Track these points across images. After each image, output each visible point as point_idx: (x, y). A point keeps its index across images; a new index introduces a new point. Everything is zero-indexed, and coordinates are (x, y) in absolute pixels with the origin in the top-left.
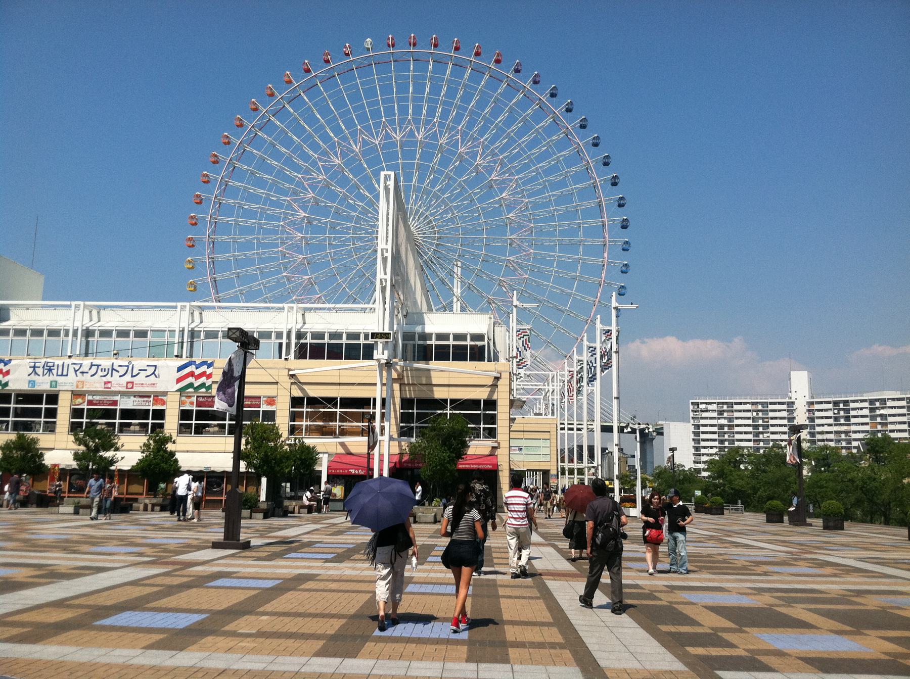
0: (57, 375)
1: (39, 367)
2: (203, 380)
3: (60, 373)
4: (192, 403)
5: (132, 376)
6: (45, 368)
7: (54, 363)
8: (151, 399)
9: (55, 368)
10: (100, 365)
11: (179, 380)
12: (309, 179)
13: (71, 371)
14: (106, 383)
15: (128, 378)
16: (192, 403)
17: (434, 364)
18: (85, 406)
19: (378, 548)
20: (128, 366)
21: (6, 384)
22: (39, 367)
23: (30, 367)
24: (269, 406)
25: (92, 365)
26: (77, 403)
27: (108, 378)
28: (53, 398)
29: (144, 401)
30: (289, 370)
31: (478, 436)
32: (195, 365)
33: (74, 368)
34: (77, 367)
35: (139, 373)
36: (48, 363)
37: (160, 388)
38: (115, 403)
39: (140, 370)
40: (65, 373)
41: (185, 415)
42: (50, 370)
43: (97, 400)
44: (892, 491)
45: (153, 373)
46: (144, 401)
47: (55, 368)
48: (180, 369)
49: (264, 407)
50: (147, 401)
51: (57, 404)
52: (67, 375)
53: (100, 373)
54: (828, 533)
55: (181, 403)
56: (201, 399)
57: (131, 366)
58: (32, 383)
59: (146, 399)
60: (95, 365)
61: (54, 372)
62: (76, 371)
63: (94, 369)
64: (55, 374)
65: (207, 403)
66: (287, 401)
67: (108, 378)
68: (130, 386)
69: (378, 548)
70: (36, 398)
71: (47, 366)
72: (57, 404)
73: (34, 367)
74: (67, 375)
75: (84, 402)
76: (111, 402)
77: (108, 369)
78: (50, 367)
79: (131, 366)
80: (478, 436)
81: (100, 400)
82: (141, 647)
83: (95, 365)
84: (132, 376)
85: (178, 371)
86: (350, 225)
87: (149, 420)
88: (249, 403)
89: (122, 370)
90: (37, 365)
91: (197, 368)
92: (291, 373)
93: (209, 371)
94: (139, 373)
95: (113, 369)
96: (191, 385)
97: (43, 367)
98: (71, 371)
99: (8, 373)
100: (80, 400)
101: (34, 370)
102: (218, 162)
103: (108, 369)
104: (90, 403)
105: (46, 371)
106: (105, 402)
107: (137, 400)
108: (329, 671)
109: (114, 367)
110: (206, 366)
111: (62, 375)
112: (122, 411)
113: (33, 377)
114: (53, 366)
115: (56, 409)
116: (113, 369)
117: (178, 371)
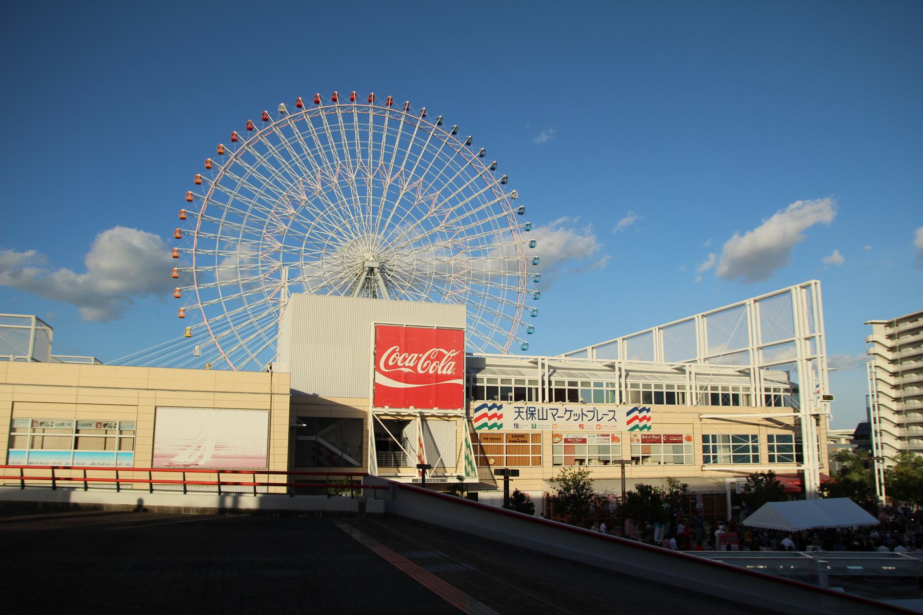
0: (539, 419)
1: (523, 412)
2: (645, 422)
3: (541, 417)
4: (638, 440)
5: (598, 420)
6: (528, 412)
7: (535, 408)
8: (610, 437)
9: (537, 412)
10: (572, 411)
11: (629, 423)
12: (343, 169)
13: (550, 416)
17: (653, 407)
20: (594, 412)
22: (523, 412)
23: (515, 412)
24: (688, 442)
26: (556, 441)
29: (605, 439)
32: (487, 407)
33: (552, 413)
34: (554, 413)
35: (603, 417)
36: (530, 408)
39: (603, 415)
40: (545, 417)
42: (532, 415)
43: (571, 439)
45: (613, 418)
46: (605, 439)
47: (537, 412)
48: (629, 413)
50: (607, 439)
51: (709, 435)
52: (547, 419)
53: (573, 418)
56: (643, 437)
57: (596, 411)
59: (606, 437)
60: (569, 411)
61: (536, 416)
62: (554, 416)
63: (568, 413)
64: (537, 418)
65: (648, 440)
68: (598, 427)
71: (529, 411)
72: (709, 435)
74: (547, 419)
75: (562, 440)
76: (581, 440)
77: (579, 414)
78: (532, 411)
79: (596, 411)
81: (573, 439)
83: (569, 411)
84: (598, 420)
85: (627, 415)
86: (342, 208)
87: (777, 442)
88: (675, 439)
90: (521, 410)
91: (489, 410)
92: (701, 416)
93: (499, 413)
94: (603, 417)
95: (583, 414)
97: (527, 412)
98: (550, 416)
101: (519, 414)
102: (236, 141)
103: (579, 414)
105: (529, 416)
106: (577, 440)
107: (600, 438)
109: (584, 412)
110: (496, 409)
111: (543, 419)
114: (535, 411)
116: (583, 414)
117: (627, 415)
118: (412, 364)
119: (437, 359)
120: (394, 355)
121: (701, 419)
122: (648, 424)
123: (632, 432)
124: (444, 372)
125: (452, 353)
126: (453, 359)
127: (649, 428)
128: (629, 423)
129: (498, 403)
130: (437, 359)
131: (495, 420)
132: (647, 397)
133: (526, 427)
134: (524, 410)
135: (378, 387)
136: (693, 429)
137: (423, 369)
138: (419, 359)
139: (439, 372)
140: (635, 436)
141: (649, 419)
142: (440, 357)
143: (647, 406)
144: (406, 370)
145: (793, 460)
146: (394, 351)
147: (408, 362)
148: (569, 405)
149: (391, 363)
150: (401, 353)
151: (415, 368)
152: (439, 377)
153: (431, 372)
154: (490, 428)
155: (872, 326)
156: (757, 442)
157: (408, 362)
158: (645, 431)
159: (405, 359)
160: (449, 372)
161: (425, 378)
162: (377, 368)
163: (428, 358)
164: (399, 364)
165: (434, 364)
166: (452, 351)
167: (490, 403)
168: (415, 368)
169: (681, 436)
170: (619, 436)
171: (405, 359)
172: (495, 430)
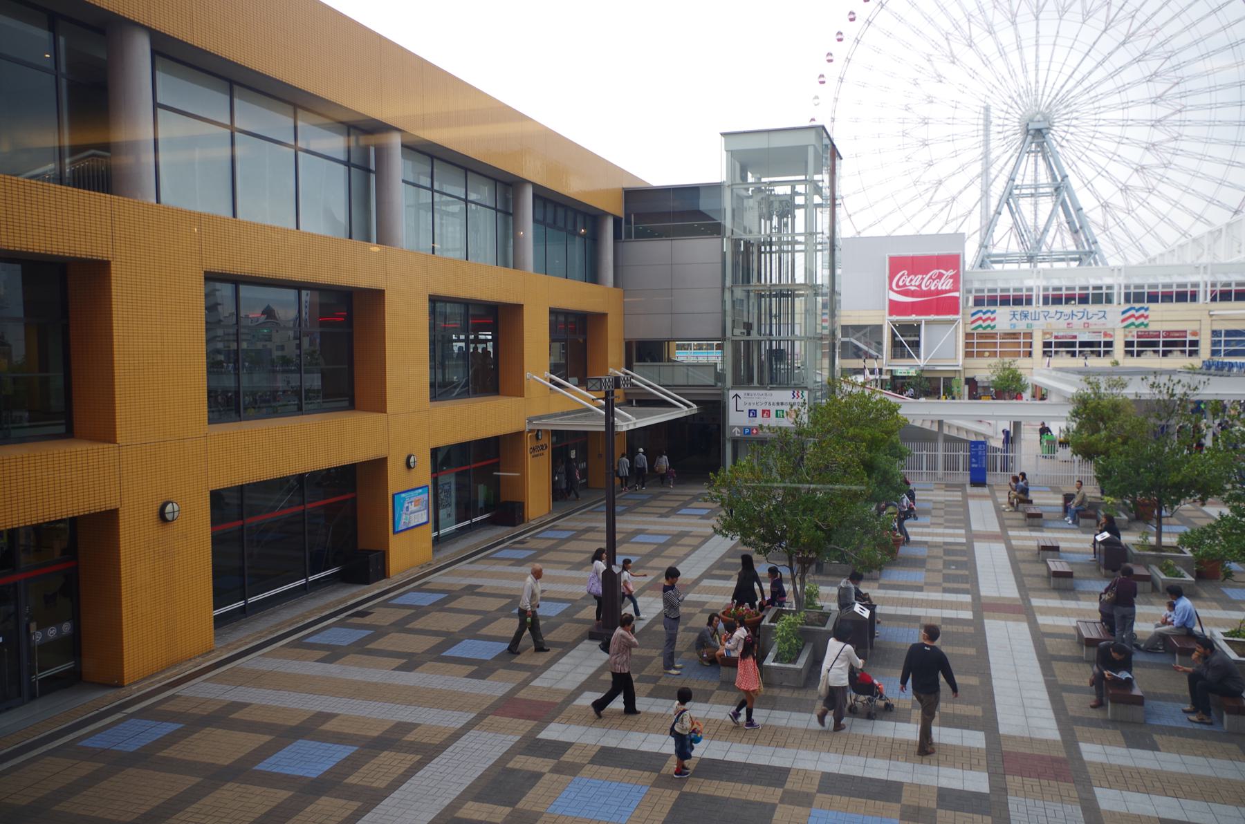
11: (1123, 321)
14: (1068, 324)
15: (1085, 319)
16: (1133, 336)
18: (1053, 340)
19: (18, 267)
21: (994, 327)
25: (1057, 312)
27: (1070, 321)
28: (1029, 335)
30: (1210, 311)
31: (1020, 356)
34: (1046, 314)
37: (1110, 325)
38: (1075, 337)
41: (1129, 344)
42: (1026, 316)
44: (1009, 369)
45: (1104, 316)
48: (1124, 313)
49: (1189, 338)
54: (1222, 399)
55: (1126, 336)
58: (1014, 326)
61: (1029, 317)
63: (1059, 315)
66: (1209, 333)
67: (1070, 321)
69: (18, 267)
70: (1014, 335)
73: (1014, 315)
80: (1020, 356)
82: (339, 718)
89: (1080, 315)
92: (1211, 313)
93: (992, 316)
96: (1133, 324)
99: (994, 319)
100: (1048, 336)
104: (1056, 337)
108: (661, 712)
112: (1080, 342)
113: (1014, 321)
115: (1044, 347)
118: (917, 284)
119: (937, 278)
120: (903, 278)
121: (1211, 316)
122: (1146, 322)
123: (1127, 330)
124: (944, 288)
125: (951, 273)
126: (951, 277)
127: (1146, 325)
128: (973, 322)
129: (1145, 305)
130: (937, 278)
131: (1142, 320)
132: (1139, 297)
133: (1021, 326)
134: (1019, 313)
135: (892, 303)
136: (1162, 321)
137: (926, 286)
138: (923, 279)
139: (939, 288)
140: (1130, 332)
141: (1146, 317)
142: (940, 276)
143: (992, 308)
144: (913, 288)
145: (880, 350)
146: (903, 275)
147: (913, 282)
148: (1024, 308)
149: (901, 283)
150: (909, 275)
151: (919, 286)
152: (938, 292)
153: (933, 288)
154: (985, 328)
155: (855, 241)
156: (1221, 332)
157: (913, 282)
158: (1142, 328)
159: (911, 280)
160: (948, 288)
161: (929, 293)
162: (891, 288)
163: (931, 278)
164: (907, 284)
165: (935, 282)
166: (901, 273)
167: (1137, 306)
168: (919, 286)
169: (1186, 331)
170: (1112, 333)
171: (911, 280)
172: (989, 330)
